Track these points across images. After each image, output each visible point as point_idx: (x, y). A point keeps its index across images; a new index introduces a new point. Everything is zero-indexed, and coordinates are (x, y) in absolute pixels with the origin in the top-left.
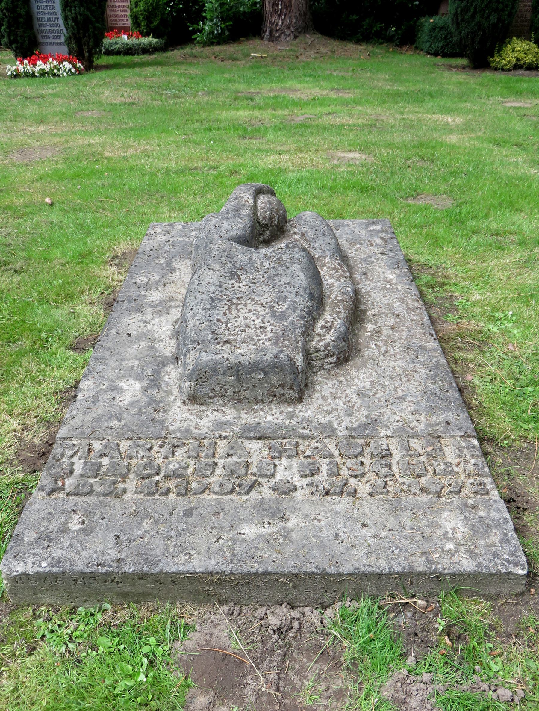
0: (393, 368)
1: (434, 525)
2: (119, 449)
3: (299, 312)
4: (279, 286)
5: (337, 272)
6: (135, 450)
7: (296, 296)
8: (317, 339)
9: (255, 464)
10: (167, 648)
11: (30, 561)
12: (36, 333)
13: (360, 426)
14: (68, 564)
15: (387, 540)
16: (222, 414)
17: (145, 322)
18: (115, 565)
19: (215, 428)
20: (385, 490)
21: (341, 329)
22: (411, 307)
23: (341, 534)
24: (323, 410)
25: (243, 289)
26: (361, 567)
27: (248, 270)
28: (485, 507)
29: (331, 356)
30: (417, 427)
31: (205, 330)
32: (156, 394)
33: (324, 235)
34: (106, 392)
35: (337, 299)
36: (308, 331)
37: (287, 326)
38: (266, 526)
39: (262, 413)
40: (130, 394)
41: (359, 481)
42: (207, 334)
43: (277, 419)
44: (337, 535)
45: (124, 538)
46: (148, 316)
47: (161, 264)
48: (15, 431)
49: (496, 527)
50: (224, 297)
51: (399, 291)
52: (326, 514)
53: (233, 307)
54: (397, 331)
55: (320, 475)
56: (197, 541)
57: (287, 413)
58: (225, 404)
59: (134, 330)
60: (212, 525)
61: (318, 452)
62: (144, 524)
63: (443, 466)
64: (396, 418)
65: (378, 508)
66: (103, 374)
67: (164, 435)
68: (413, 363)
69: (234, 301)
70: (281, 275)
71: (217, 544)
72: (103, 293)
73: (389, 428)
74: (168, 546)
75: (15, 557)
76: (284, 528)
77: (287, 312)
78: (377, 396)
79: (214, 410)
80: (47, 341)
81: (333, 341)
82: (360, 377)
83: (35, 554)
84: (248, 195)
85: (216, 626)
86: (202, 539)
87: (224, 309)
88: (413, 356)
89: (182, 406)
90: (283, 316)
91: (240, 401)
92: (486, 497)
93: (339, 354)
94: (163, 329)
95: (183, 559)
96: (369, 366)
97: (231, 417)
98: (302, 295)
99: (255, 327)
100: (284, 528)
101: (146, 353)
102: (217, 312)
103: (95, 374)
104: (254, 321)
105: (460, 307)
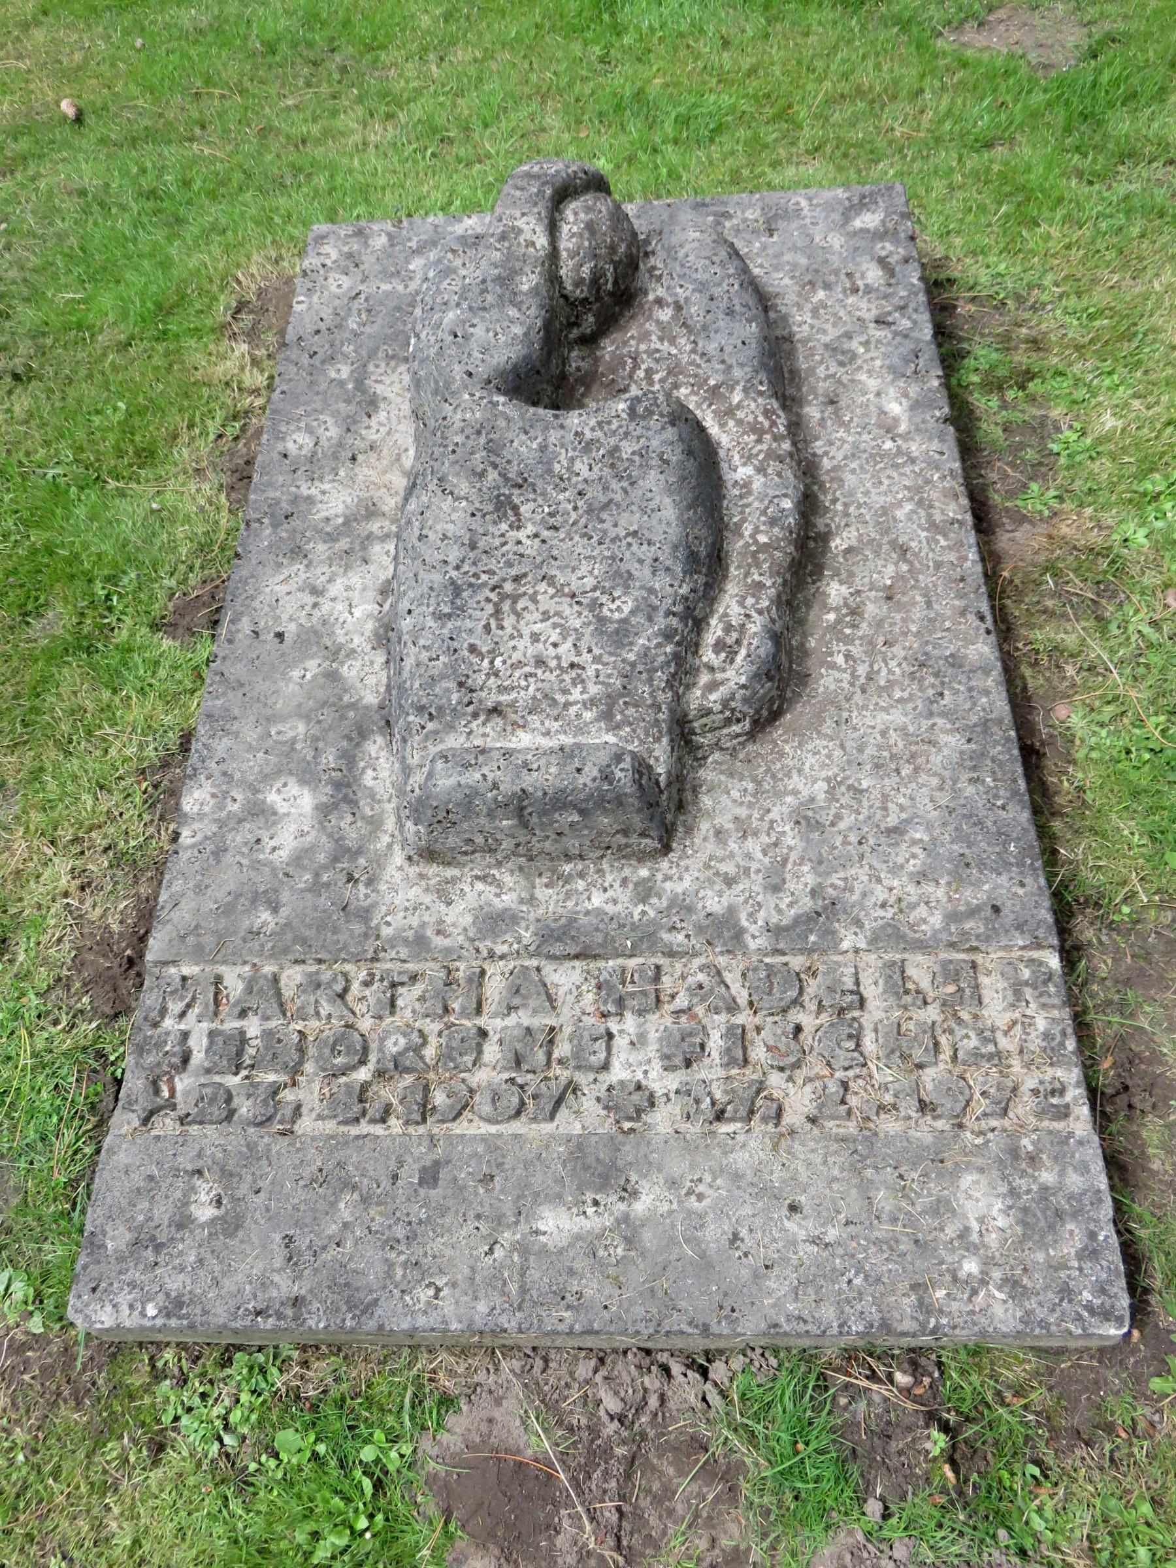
0: (884, 734)
1: (941, 1208)
2: (279, 994)
3: (661, 622)
4: (613, 540)
5: (759, 441)
6: (312, 999)
7: (654, 573)
8: (704, 678)
9: (568, 1031)
10: (407, 1449)
11: (124, 1299)
12: (80, 584)
13: (796, 921)
14: (198, 1311)
15: (840, 1251)
16: (494, 890)
17: (315, 591)
18: (289, 1312)
19: (480, 931)
20: (843, 1109)
21: (762, 652)
22: (938, 518)
23: (744, 1233)
24: (717, 874)
25: (531, 547)
26: (782, 1320)
27: (540, 484)
28: (1056, 1159)
29: (738, 721)
30: (925, 921)
31: (443, 677)
32: (350, 829)
33: (730, 312)
34: (240, 821)
35: (756, 542)
36: (683, 668)
37: (633, 665)
38: (590, 1211)
39: (581, 885)
40: (293, 828)
41: (790, 1079)
42: (447, 690)
43: (615, 902)
44: (736, 1237)
45: (302, 1243)
46: (319, 571)
47: (342, 383)
48: (66, 895)
49: (1075, 1214)
50: (484, 577)
51: (913, 461)
52: (714, 1179)
53: (506, 606)
54: (900, 607)
55: (706, 1061)
56: (449, 1252)
57: (636, 885)
58: (499, 864)
59: (291, 619)
60: (479, 1209)
61: (703, 1000)
62: (342, 1205)
63: (974, 1042)
64: (880, 894)
65: (825, 1162)
66: (231, 766)
67: (370, 955)
68: (931, 714)
69: (508, 587)
70: (618, 506)
71: (489, 1260)
72: (220, 436)
73: (862, 927)
74: (391, 1265)
75: (94, 1290)
76: (626, 1218)
77: (634, 621)
78: (842, 825)
79: (477, 878)
80: (110, 609)
81: (744, 687)
82: (806, 762)
83: (132, 1285)
84: (532, 219)
85: (498, 1402)
86: (457, 1244)
87: (485, 614)
88: (931, 692)
89: (406, 864)
90: (620, 635)
91: (530, 859)
92: (1059, 1125)
93: (758, 712)
94: (358, 612)
95: (423, 1298)
96: (828, 727)
97: (514, 895)
98: (668, 569)
99: (559, 666)
100: (626, 1218)
101: (320, 695)
102: (468, 624)
103: (213, 765)
104: (555, 645)
105: (1063, 460)
